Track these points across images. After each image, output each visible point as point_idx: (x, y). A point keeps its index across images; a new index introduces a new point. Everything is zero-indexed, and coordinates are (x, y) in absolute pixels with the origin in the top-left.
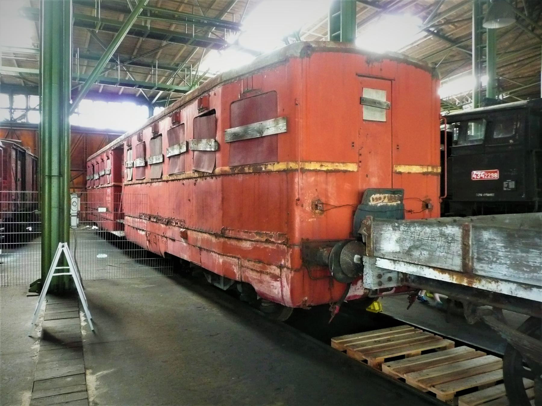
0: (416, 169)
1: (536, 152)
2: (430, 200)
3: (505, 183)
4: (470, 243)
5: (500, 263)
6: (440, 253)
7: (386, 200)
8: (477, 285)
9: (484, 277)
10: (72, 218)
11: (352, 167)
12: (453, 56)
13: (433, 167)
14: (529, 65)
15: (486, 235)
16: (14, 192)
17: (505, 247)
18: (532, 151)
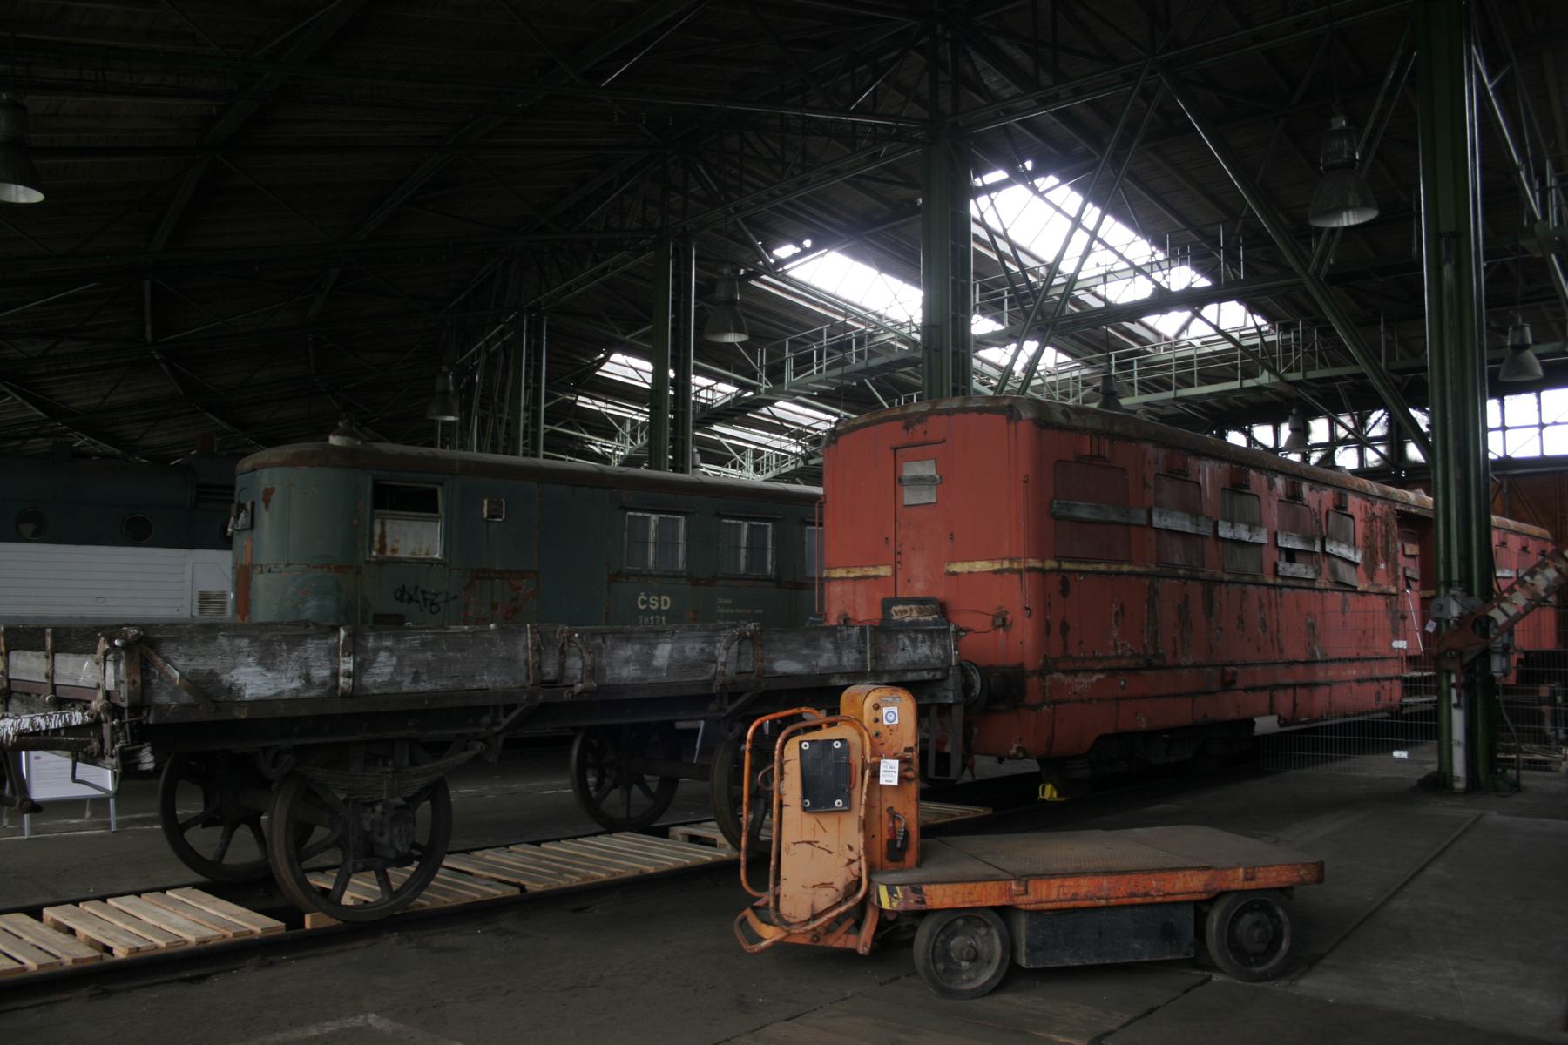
0: (981, 566)
7: (915, 614)
10: (1490, 434)
11: (885, 571)
13: (1011, 560)
16: (1173, 372)
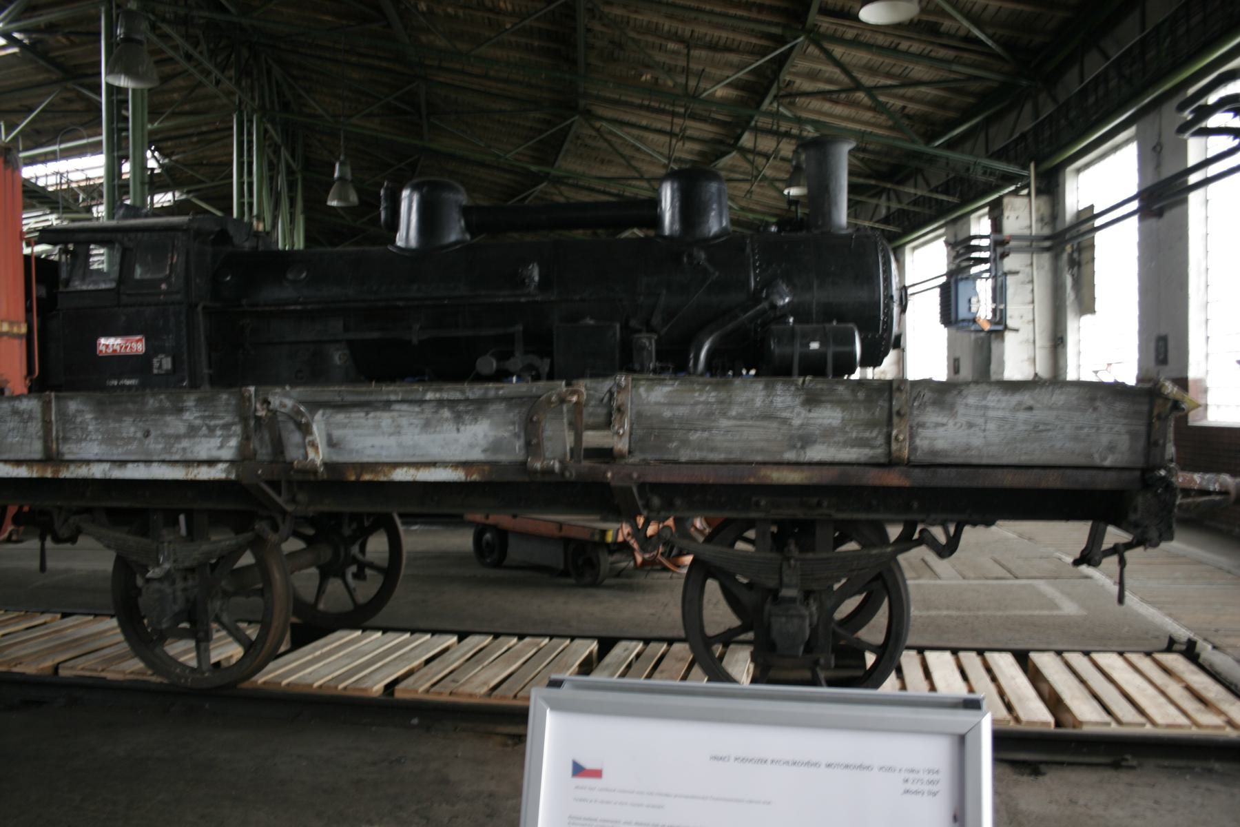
1: (204, 308)
2: (7, 382)
4: (53, 418)
6: (14, 439)
12: (69, 101)
13: (11, 323)
15: (72, 406)
17: (96, 419)
18: (196, 306)
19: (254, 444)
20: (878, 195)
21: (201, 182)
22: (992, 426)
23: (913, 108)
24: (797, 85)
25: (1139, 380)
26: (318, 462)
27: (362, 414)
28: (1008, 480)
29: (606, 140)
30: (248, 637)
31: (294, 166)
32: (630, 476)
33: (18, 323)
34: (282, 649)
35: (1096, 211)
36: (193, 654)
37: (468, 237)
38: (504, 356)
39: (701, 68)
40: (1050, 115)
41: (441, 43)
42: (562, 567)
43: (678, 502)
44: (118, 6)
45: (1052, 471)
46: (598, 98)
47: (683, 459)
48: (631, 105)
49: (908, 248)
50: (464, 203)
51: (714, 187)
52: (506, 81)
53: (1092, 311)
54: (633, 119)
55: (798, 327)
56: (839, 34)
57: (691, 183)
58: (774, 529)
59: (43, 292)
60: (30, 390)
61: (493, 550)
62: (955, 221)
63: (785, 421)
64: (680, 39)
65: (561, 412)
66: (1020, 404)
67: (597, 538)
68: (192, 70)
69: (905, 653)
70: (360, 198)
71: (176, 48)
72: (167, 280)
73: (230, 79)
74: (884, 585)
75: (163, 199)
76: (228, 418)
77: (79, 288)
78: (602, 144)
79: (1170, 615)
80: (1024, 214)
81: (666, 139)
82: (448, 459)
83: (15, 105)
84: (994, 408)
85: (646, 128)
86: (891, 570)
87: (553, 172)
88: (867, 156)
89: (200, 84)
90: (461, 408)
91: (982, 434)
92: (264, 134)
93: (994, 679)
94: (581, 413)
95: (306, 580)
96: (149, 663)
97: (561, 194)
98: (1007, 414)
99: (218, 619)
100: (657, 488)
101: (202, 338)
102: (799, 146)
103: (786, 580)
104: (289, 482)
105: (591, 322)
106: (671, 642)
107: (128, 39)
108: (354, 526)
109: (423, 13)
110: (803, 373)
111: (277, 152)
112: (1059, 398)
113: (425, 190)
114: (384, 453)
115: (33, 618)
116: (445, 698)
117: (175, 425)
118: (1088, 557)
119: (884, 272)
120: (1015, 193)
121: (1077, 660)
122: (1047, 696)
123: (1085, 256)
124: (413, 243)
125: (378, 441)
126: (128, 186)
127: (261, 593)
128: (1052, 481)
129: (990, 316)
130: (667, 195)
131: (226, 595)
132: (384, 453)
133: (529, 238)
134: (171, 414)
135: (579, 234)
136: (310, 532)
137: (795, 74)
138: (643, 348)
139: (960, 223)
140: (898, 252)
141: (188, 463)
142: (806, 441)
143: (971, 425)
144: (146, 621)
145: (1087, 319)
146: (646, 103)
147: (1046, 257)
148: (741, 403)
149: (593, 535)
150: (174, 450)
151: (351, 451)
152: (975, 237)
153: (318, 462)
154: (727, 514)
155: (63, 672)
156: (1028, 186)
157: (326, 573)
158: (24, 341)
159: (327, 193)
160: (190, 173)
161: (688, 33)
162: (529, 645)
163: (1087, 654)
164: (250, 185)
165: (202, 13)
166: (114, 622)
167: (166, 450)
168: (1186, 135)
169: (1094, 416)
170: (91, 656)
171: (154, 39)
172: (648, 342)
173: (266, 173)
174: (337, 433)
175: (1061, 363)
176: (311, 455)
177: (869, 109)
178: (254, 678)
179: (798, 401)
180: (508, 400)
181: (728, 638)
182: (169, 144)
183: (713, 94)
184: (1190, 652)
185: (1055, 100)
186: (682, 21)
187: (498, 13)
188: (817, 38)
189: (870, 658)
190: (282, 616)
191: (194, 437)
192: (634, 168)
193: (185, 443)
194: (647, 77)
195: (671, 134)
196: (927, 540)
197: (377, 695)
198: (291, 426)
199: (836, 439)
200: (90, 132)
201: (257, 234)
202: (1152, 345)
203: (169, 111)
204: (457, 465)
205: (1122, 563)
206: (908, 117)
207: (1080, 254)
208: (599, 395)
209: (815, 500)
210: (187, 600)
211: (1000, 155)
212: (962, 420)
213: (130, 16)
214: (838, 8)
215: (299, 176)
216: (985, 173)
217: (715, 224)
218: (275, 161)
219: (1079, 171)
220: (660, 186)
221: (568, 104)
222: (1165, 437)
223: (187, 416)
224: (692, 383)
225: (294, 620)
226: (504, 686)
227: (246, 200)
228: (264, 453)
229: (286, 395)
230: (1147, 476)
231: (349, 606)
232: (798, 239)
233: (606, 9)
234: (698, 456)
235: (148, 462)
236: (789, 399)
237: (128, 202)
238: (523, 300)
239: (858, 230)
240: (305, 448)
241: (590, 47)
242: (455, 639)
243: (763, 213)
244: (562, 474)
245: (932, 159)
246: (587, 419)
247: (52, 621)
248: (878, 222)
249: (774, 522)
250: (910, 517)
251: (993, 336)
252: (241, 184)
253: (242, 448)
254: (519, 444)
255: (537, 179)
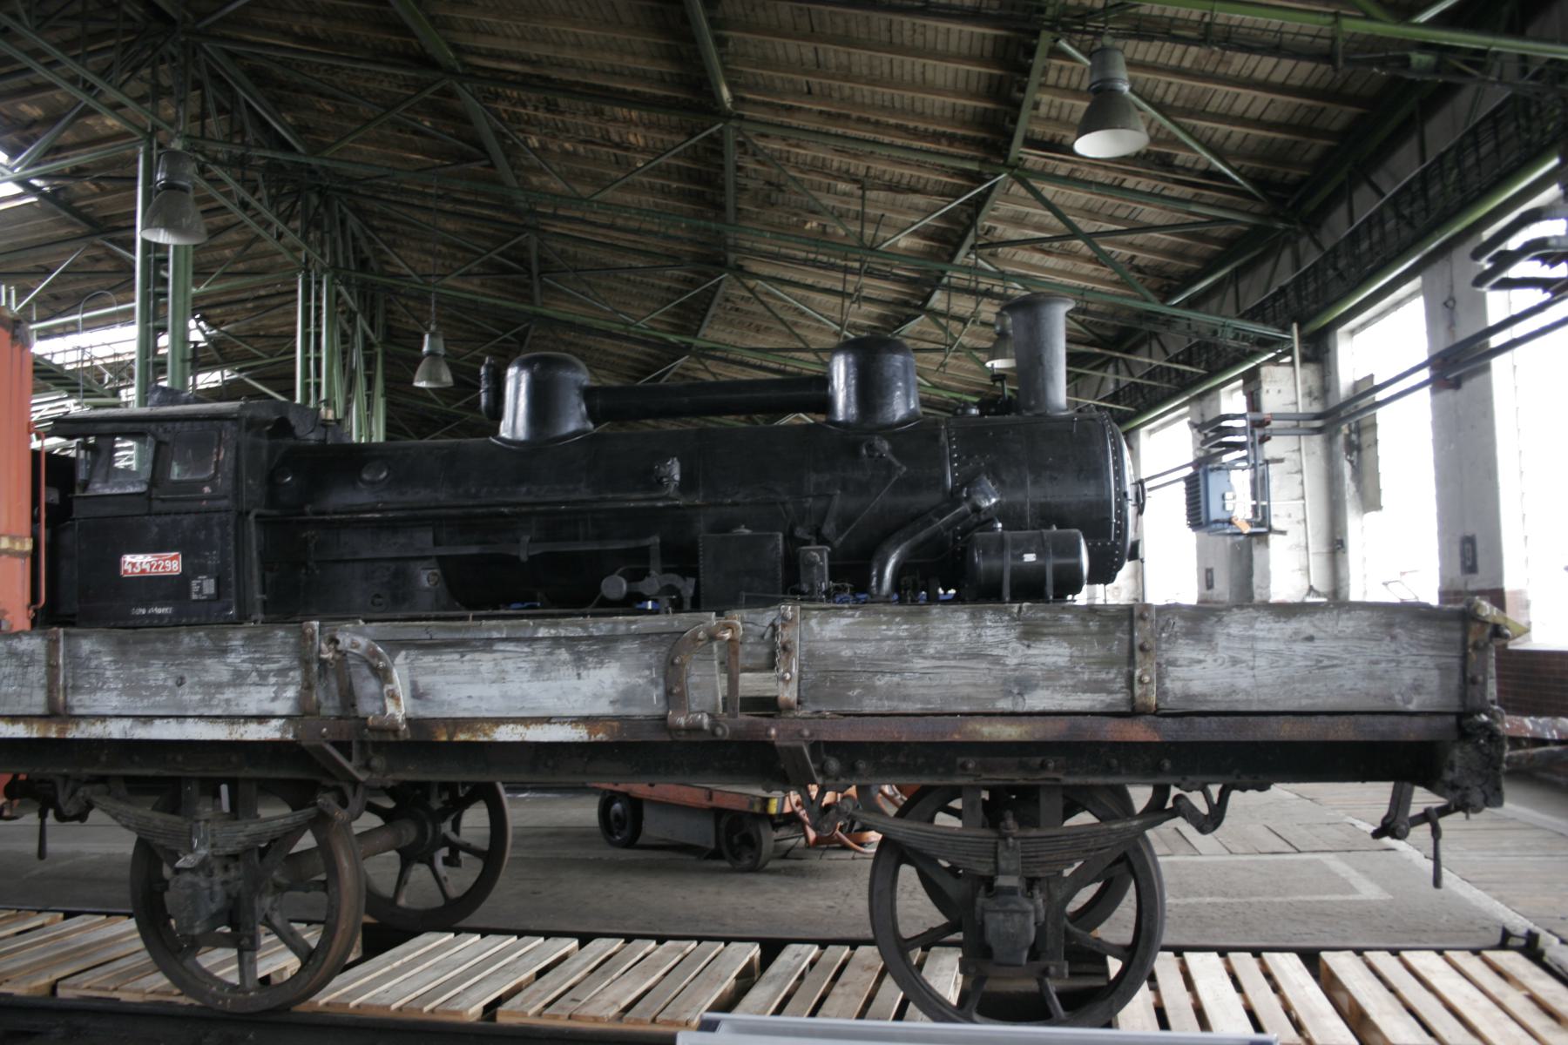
1: (257, 516)
3: (194, 583)
5: (109, 690)
8: (74, 733)
9: (83, 717)
12: (97, 260)
13: (13, 538)
14: (280, 310)
15: (86, 646)
17: (115, 662)
18: (248, 513)
19: (318, 694)
20: (1103, 366)
21: (257, 358)
22: (1262, 662)
23: (1144, 258)
24: (999, 232)
25: (1444, 594)
26: (400, 718)
27: (457, 656)
28: (1286, 731)
29: (762, 302)
30: (305, 943)
31: (372, 337)
32: (800, 733)
33: (21, 538)
34: (352, 958)
35: (1377, 382)
36: (235, 966)
37: (590, 425)
38: (636, 576)
39: (880, 212)
40: (1315, 266)
41: (557, 185)
42: (712, 846)
43: (862, 765)
44: (160, 146)
45: (1343, 718)
46: (751, 251)
47: (867, 710)
48: (792, 259)
49: (1143, 431)
50: (586, 383)
51: (898, 360)
52: (637, 232)
53: (1378, 507)
54: (796, 277)
55: (1008, 534)
56: (1049, 169)
57: (869, 353)
58: (985, 795)
59: (55, 496)
60: (34, 623)
61: (623, 825)
62: (1200, 397)
63: (997, 660)
64: (854, 180)
65: (711, 652)
66: (1296, 633)
67: (757, 809)
68: (248, 221)
69: (1160, 954)
70: (454, 376)
71: (228, 194)
72: (211, 481)
73: (295, 231)
74: (1128, 868)
75: (209, 379)
76: (285, 662)
77: (101, 492)
78: (756, 307)
79: (1500, 899)
80: (1287, 387)
81: (837, 300)
82: (566, 714)
83: (30, 266)
84: (1263, 639)
85: (811, 288)
86: (1138, 850)
87: (697, 343)
88: (1089, 318)
89: (258, 238)
90: (583, 648)
91: (1250, 673)
92: (335, 300)
93: (1276, 989)
94: (736, 653)
95: (383, 869)
96: (176, 980)
97: (707, 370)
98: (1282, 647)
99: (267, 922)
100: (834, 748)
101: (255, 554)
102: (1003, 309)
103: (1003, 864)
104: (363, 744)
105: (747, 532)
106: (854, 944)
107: (170, 186)
108: (446, 796)
109: (533, 150)
110: (1014, 599)
111: (351, 321)
112: (1347, 624)
113: (536, 367)
114: (484, 705)
115: (26, 919)
116: (562, 1023)
117: (218, 670)
118: (1389, 828)
119: (1115, 463)
120: (1274, 361)
121: (1383, 961)
122: (1346, 1009)
123: (1366, 438)
124: (522, 434)
125: (476, 690)
126: (164, 364)
127: (324, 886)
128: (1342, 731)
129: (1249, 516)
130: (841, 372)
131: (279, 888)
132: (484, 705)
133: (669, 425)
134: (212, 656)
135: (729, 420)
136: (389, 804)
137: (997, 219)
138: (812, 564)
139: (1207, 399)
140: (1130, 435)
141: (232, 719)
142: (1025, 685)
143: (1235, 662)
144: (173, 922)
145: (1372, 516)
146: (812, 256)
147: (1317, 440)
148: (940, 639)
149: (752, 804)
150: (215, 702)
151: (442, 703)
152: (1227, 417)
153: (400, 718)
154: (926, 781)
155: (62, 993)
156: (1290, 352)
157: (409, 857)
158: (28, 561)
159: (414, 370)
160: (245, 346)
161: (862, 171)
162: (672, 950)
163: (1395, 952)
164: (318, 361)
165: (262, 153)
166: (131, 924)
167: (205, 702)
168: (1485, 289)
169: (1393, 646)
170: (100, 970)
171: (203, 184)
172: (819, 556)
173: (338, 347)
174: (424, 681)
175: (1342, 573)
176: (391, 709)
177: (1090, 260)
178: (314, 999)
179: (1013, 634)
180: (642, 636)
181: (931, 940)
182: (218, 311)
183: (895, 245)
184: (1531, 949)
185: (1319, 246)
186: (855, 156)
187: (627, 149)
188: (1022, 175)
189: (1115, 966)
190: (352, 915)
191: (241, 685)
192: (798, 337)
193: (229, 694)
194: (812, 225)
195: (843, 294)
196: (1182, 809)
197: (472, 1020)
198: (366, 671)
199: (1063, 682)
200: (121, 297)
201: (325, 424)
202: (1456, 549)
203: (219, 271)
204: (578, 721)
205: (1436, 833)
206: (1139, 269)
207: (1359, 436)
208: (759, 630)
209: (1038, 760)
210: (229, 896)
211: (1255, 314)
212: (1223, 654)
213: (173, 156)
214: (1047, 139)
215: (379, 350)
216: (1235, 338)
217: (900, 406)
218: (349, 332)
219: (1353, 332)
220: (831, 360)
221: (714, 259)
222: (1484, 671)
223: (232, 658)
224: (878, 613)
225: (368, 919)
226: (639, 1006)
227: (312, 380)
228: (330, 707)
229: (360, 633)
230: (1463, 724)
231: (440, 902)
232: (1003, 421)
233: (761, 143)
234: (886, 706)
235: (181, 718)
236: (1002, 631)
237: (165, 384)
238: (660, 504)
239: (1080, 411)
240: (383, 700)
241: (742, 189)
242: (575, 943)
243: (961, 391)
244: (713, 733)
245: (1169, 321)
246: (743, 661)
247: (51, 923)
248: (1103, 400)
249: (986, 788)
250: (1161, 780)
251: (1254, 540)
252: (306, 361)
253: (301, 700)
254: (657, 693)
255: (677, 351)
